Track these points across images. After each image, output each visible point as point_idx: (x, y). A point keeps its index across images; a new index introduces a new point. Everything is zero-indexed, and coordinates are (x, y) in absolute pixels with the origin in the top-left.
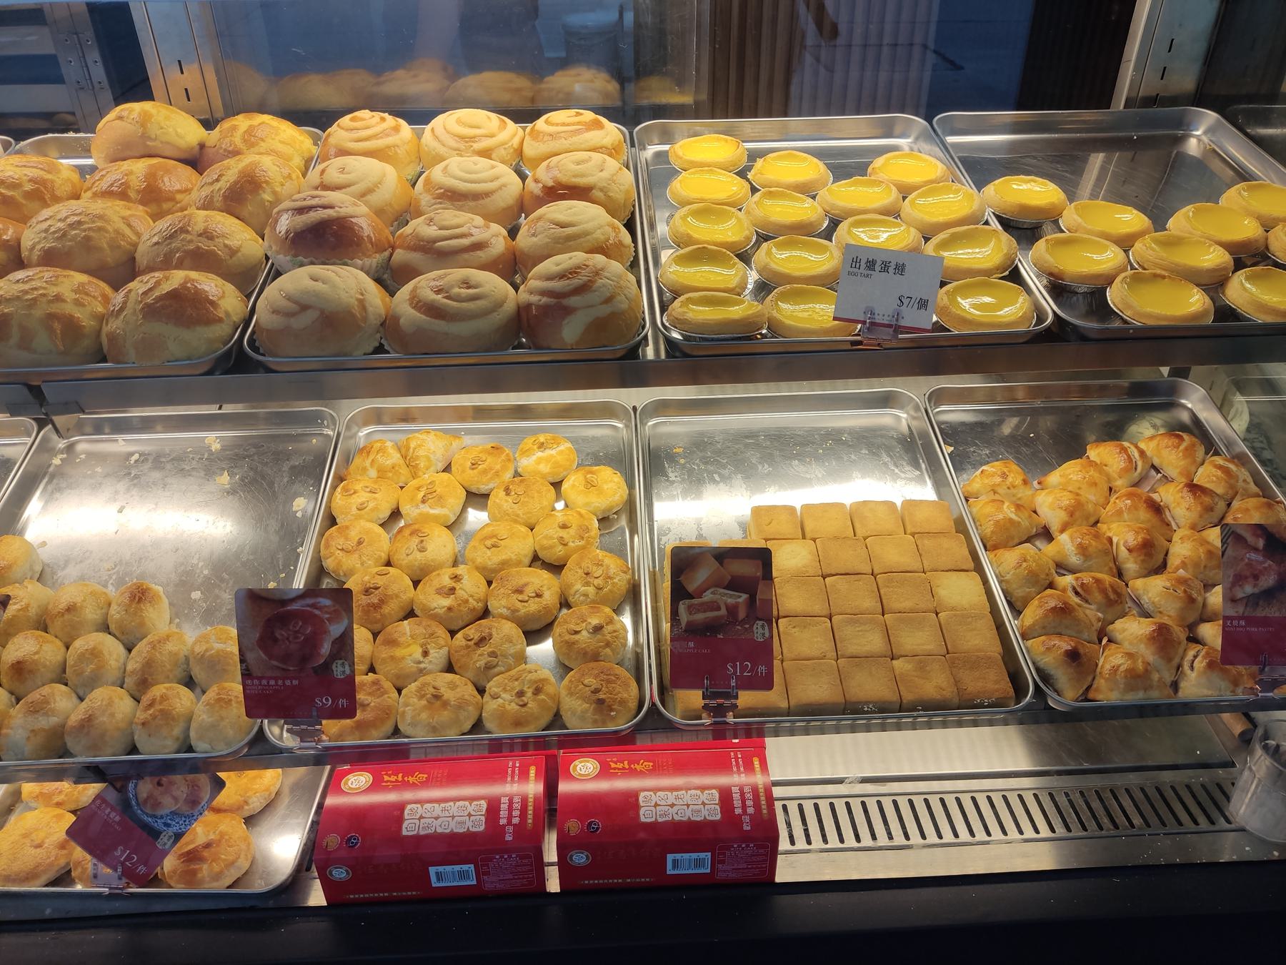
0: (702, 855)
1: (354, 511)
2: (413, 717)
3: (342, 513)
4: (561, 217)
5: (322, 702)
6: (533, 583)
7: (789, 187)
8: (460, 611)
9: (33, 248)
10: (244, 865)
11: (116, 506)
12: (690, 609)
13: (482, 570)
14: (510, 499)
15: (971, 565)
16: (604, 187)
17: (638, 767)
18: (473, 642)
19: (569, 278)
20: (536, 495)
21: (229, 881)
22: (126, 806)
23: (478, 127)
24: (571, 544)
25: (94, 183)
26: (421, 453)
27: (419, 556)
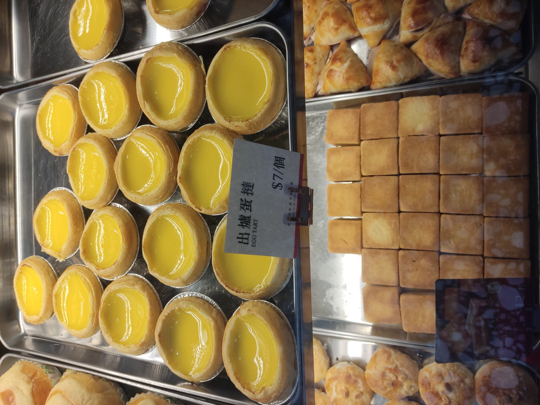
15: (393, 103)
24: (362, 389)
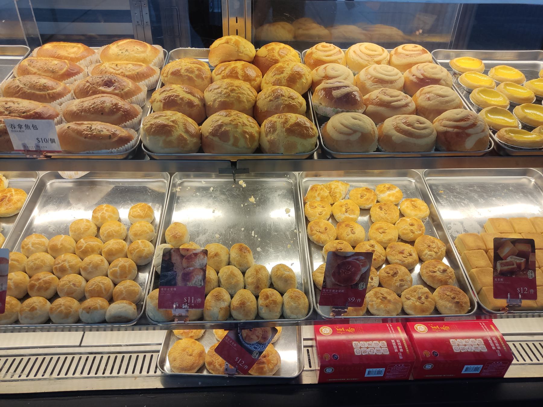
0: (381, 369)
1: (318, 215)
2: (377, 307)
3: (312, 216)
4: (441, 92)
5: (351, 299)
6: (407, 249)
7: (512, 81)
8: (379, 260)
9: (215, 100)
10: (276, 369)
11: (211, 210)
12: (502, 264)
13: (380, 243)
14: (383, 212)
16: (445, 79)
17: (349, 331)
18: (390, 275)
19: (465, 121)
20: (393, 211)
21: (274, 373)
22: (238, 340)
23: (375, 51)
25: (221, 72)
26: (337, 190)
27: (353, 235)
